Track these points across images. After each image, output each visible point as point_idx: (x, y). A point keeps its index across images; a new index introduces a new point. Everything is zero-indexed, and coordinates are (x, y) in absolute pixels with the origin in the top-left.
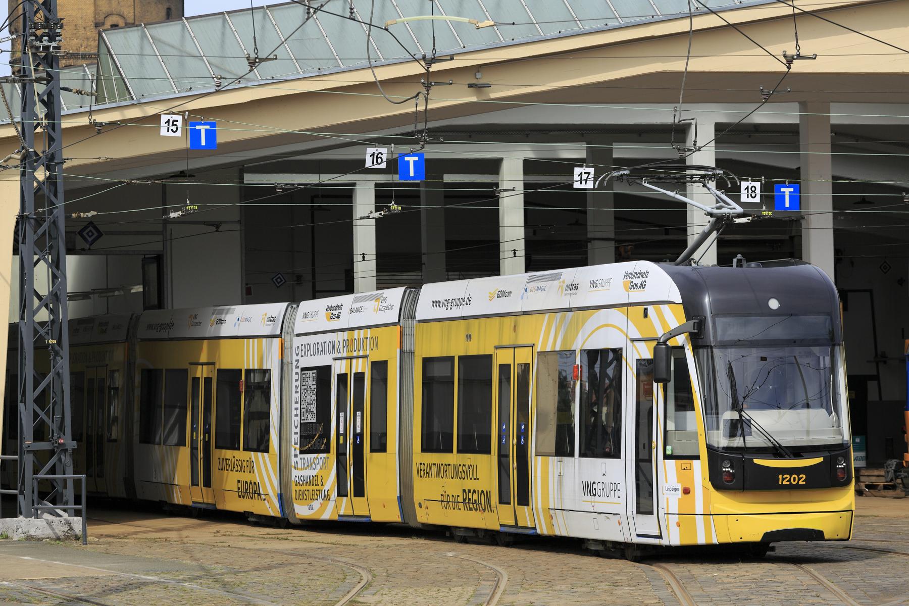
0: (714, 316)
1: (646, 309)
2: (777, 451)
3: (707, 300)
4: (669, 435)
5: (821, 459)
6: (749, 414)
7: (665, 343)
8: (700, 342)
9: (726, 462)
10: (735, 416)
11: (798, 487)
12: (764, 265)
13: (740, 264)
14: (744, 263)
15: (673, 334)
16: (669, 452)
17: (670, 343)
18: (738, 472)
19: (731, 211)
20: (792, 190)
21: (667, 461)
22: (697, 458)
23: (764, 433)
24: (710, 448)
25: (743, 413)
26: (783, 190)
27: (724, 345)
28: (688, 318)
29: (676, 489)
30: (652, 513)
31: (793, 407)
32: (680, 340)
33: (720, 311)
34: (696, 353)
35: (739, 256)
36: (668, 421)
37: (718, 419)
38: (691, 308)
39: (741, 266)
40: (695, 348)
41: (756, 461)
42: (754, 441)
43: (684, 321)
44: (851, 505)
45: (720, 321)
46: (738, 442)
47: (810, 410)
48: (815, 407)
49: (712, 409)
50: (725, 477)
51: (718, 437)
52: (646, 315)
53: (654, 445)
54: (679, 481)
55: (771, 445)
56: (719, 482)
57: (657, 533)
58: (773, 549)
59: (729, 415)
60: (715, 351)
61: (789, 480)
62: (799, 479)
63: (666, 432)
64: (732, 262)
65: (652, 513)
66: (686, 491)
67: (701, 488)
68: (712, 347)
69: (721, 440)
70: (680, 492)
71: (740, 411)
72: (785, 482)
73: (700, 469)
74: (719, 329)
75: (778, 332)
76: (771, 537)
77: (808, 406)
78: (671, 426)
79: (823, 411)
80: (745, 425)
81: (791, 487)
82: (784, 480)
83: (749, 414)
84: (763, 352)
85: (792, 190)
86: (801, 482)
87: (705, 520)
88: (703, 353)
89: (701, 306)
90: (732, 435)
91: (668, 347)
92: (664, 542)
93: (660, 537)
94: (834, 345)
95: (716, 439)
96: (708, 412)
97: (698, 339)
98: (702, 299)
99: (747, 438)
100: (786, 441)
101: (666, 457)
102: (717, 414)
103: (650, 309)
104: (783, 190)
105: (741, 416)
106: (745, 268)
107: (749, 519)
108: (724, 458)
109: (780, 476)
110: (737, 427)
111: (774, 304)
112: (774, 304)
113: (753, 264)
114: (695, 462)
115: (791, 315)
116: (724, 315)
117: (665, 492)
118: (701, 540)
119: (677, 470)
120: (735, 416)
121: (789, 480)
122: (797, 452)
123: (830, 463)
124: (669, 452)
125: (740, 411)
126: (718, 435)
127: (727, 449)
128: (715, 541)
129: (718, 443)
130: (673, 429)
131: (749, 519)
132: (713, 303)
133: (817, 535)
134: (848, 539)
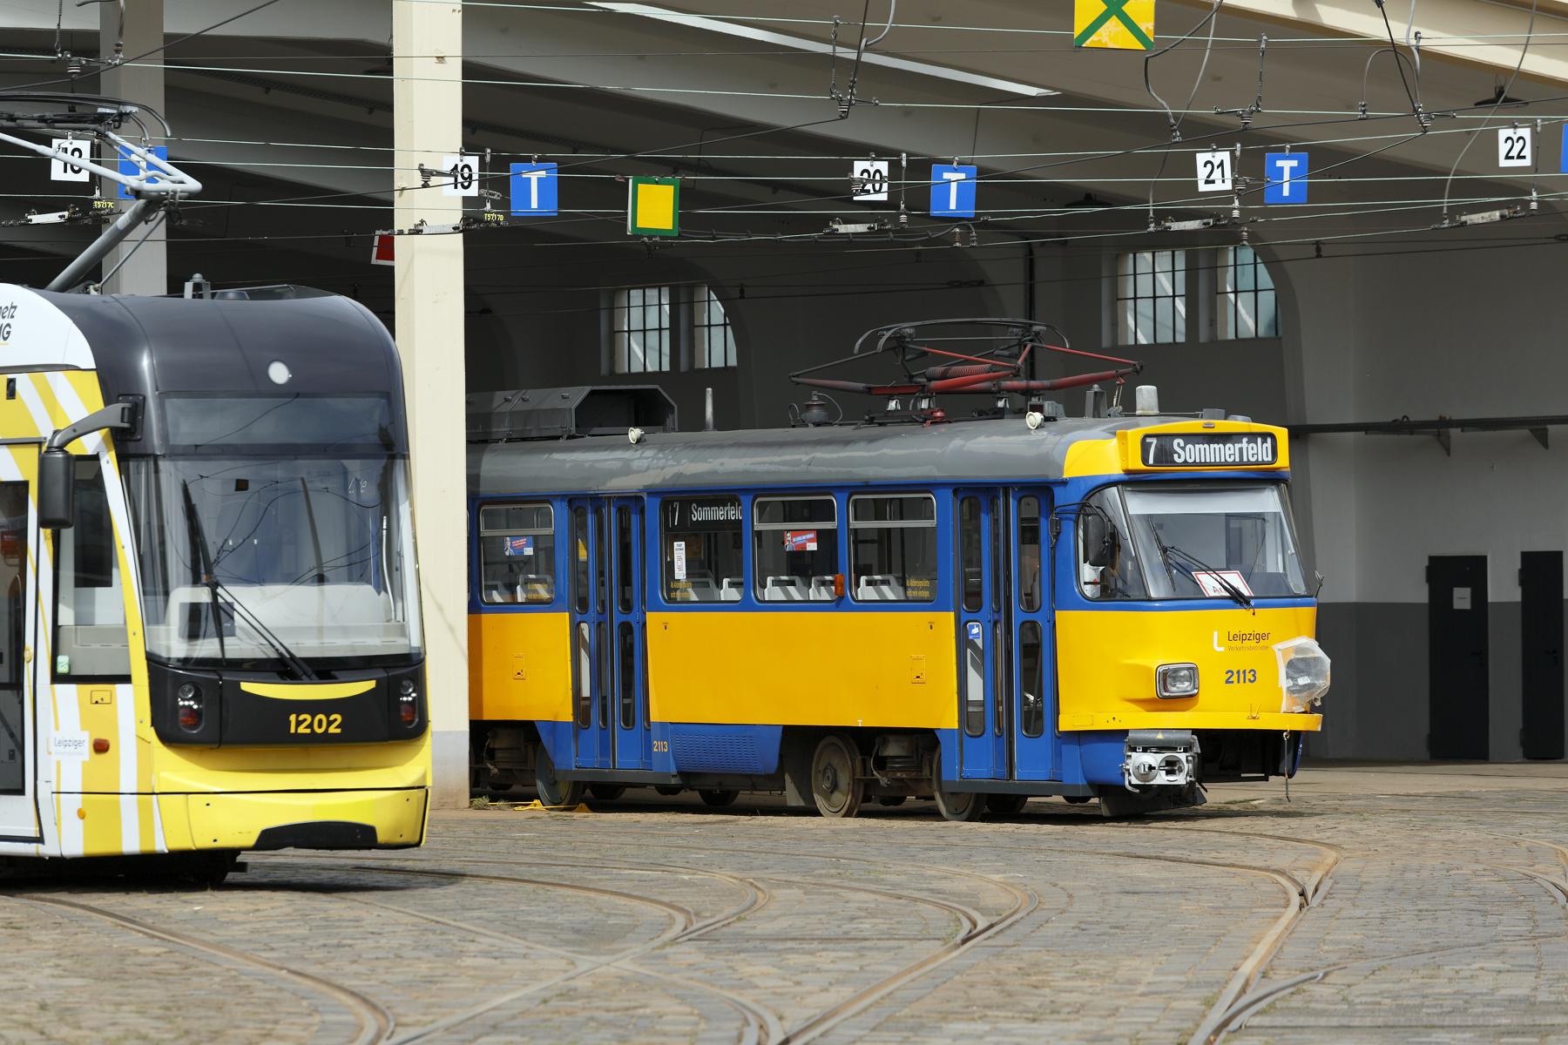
0: (163, 395)
1: (11, 382)
2: (285, 667)
3: (145, 363)
4: (63, 634)
5: (369, 685)
6: (233, 593)
7: (61, 448)
8: (132, 448)
9: (187, 687)
10: (203, 595)
11: (326, 738)
12: (254, 296)
13: (198, 293)
14: (207, 292)
15: (78, 431)
16: (63, 668)
17: (74, 448)
18: (209, 709)
19: (179, 187)
20: (1295, 163)
21: (58, 687)
22: (126, 679)
23: (261, 631)
24: (153, 660)
25: (219, 590)
26: (1279, 163)
27: (175, 453)
28: (108, 399)
29: (78, 744)
30: (21, 792)
31: (294, 579)
32: (89, 444)
33: (176, 384)
34: (123, 470)
35: (197, 277)
36: (61, 607)
37: (166, 601)
38: (114, 378)
39: (201, 297)
40: (123, 460)
41: (246, 687)
42: (240, 646)
43: (98, 403)
44: (424, 777)
45: (172, 404)
46: (207, 648)
47: (327, 588)
48: (338, 581)
49: (155, 583)
50: (182, 717)
51: (168, 638)
52: (11, 393)
53: (28, 653)
54: (85, 724)
55: (274, 655)
56: (170, 728)
57: (32, 831)
58: (242, 867)
59: (184, 594)
60: (162, 464)
61: (310, 726)
62: (330, 723)
63: (56, 627)
64: (182, 290)
65: (21, 792)
66: (101, 747)
67: (134, 739)
68: (156, 458)
69: (175, 646)
70: (87, 748)
71: (214, 586)
72: (301, 730)
73: (131, 704)
74: (163, 423)
75: (267, 430)
76: (272, 839)
77: (321, 579)
78: (67, 616)
79: (368, 589)
80: (222, 614)
81: (313, 740)
82: (300, 725)
83: (233, 593)
84: (242, 470)
85: (1295, 163)
86: (332, 730)
87: (141, 807)
88: (142, 470)
89: (133, 375)
90: (193, 634)
91: (68, 457)
92: (48, 849)
93: (40, 840)
94: (393, 457)
95: (163, 643)
96: (149, 588)
97: (127, 441)
98: (141, 359)
99: (227, 640)
100: (306, 647)
101: (57, 678)
102: (167, 593)
103: (22, 380)
104: (1279, 163)
105: (215, 595)
106: (207, 300)
107: (228, 804)
108: (179, 682)
109: (293, 718)
110: (196, 623)
111: (279, 373)
112: (279, 373)
113: (231, 293)
114: (120, 688)
115: (298, 395)
116: (179, 394)
117: (53, 749)
118: (131, 843)
119: (81, 705)
120: (203, 595)
121: (310, 726)
122: (325, 669)
123: (387, 694)
124: (63, 668)
125: (214, 586)
126: (168, 632)
127: (185, 662)
128: (161, 845)
129: (169, 649)
130: (72, 622)
131: (228, 804)
132: (161, 370)
133: (358, 836)
134: (418, 844)
